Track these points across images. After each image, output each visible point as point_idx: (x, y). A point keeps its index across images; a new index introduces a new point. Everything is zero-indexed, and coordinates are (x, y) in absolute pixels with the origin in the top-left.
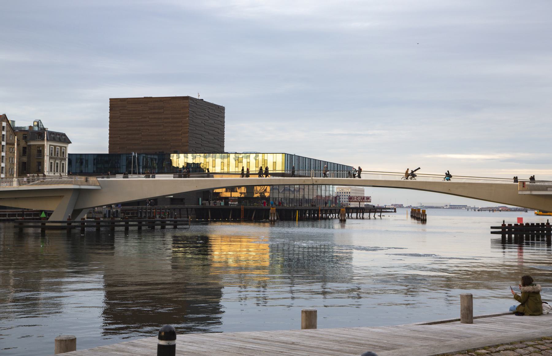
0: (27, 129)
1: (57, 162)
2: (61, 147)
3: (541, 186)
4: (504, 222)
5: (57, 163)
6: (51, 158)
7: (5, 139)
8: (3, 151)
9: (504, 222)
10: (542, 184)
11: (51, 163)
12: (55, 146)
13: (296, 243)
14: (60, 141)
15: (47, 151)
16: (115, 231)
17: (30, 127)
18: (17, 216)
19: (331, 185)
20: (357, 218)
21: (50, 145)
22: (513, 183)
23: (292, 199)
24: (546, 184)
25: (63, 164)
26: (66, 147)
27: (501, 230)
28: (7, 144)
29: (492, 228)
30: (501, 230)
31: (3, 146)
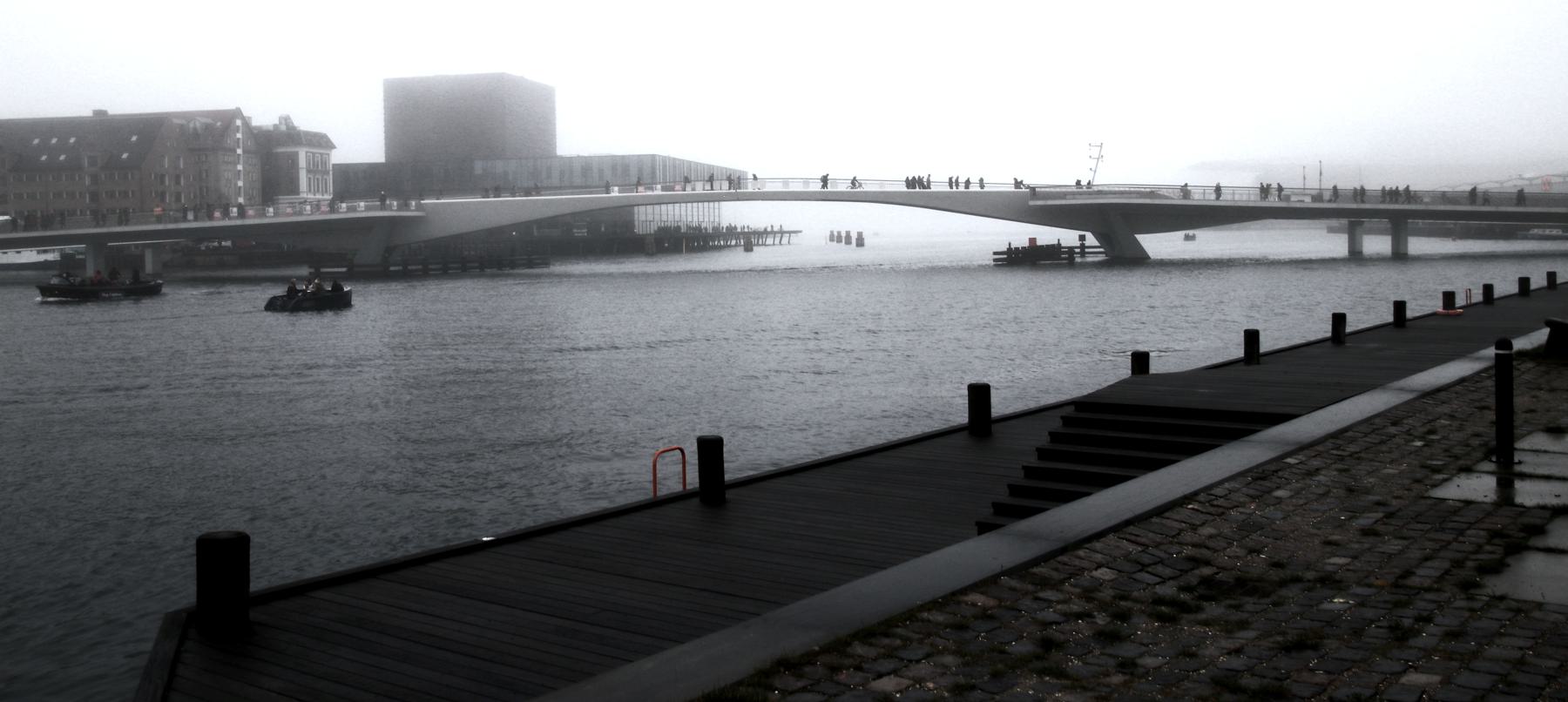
0: (271, 128)
1: (317, 176)
2: (321, 154)
3: (1057, 192)
4: (1010, 244)
5: (318, 179)
6: (309, 171)
7: (241, 145)
8: (239, 179)
9: (1010, 244)
10: (1058, 190)
11: (310, 178)
12: (314, 154)
13: (207, 247)
14: (320, 146)
15: (302, 162)
16: (1516, 449)
17: (275, 126)
18: (190, 216)
19: (677, 203)
20: (774, 244)
21: (307, 152)
22: (1013, 189)
23: (643, 221)
24: (1064, 190)
25: (326, 180)
26: (328, 154)
27: (1005, 256)
28: (244, 152)
29: (995, 253)
30: (1005, 256)
31: (239, 155)
